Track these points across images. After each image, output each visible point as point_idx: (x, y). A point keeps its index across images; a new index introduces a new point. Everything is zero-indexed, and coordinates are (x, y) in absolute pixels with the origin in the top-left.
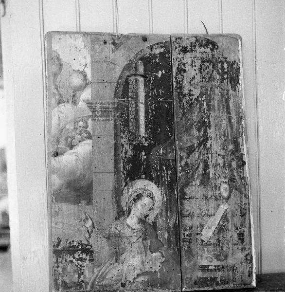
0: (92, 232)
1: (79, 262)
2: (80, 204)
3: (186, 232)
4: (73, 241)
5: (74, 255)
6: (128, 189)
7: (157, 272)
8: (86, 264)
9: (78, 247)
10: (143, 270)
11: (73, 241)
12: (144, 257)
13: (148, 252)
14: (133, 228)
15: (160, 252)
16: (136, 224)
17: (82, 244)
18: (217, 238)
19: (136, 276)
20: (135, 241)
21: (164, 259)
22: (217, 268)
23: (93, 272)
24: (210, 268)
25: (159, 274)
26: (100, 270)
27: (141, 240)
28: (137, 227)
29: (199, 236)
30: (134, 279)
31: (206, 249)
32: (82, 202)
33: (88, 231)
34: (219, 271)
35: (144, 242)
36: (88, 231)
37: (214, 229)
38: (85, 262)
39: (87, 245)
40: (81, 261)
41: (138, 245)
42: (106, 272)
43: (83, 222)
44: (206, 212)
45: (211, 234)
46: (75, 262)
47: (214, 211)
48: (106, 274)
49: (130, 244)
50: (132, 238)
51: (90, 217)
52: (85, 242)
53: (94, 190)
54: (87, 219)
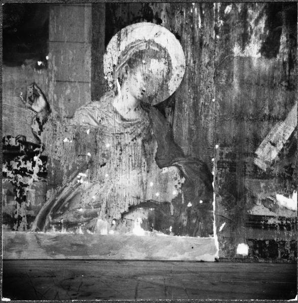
0: (45, 121)
1: (19, 176)
2: (23, 66)
3: (226, 148)
4: (9, 137)
5: (9, 163)
6: (119, 40)
7: (169, 204)
8: (32, 180)
9: (18, 148)
10: (142, 198)
11: (9, 137)
12: (144, 174)
13: (154, 165)
14: (126, 117)
15: (176, 166)
16: (132, 111)
17: (24, 142)
18: (286, 164)
19: (126, 209)
20: (127, 142)
21: (183, 180)
22: (284, 222)
23: (45, 197)
24: (271, 221)
25: (172, 207)
26: (59, 194)
27: (139, 141)
28: (133, 115)
29: (249, 158)
30: (123, 215)
31: (262, 185)
32: (27, 61)
33: (38, 119)
34: (289, 229)
35: (139, 216)
36: (38, 119)
37: (281, 147)
38: (31, 177)
39: (35, 146)
40: (23, 175)
41: (133, 149)
42: (68, 199)
43: (28, 100)
44: (266, 112)
45: (274, 155)
46: (12, 176)
47: (283, 110)
48: (70, 201)
49: (119, 149)
50: (123, 136)
51: (42, 93)
52: (31, 139)
53: (51, 39)
54: (37, 96)
